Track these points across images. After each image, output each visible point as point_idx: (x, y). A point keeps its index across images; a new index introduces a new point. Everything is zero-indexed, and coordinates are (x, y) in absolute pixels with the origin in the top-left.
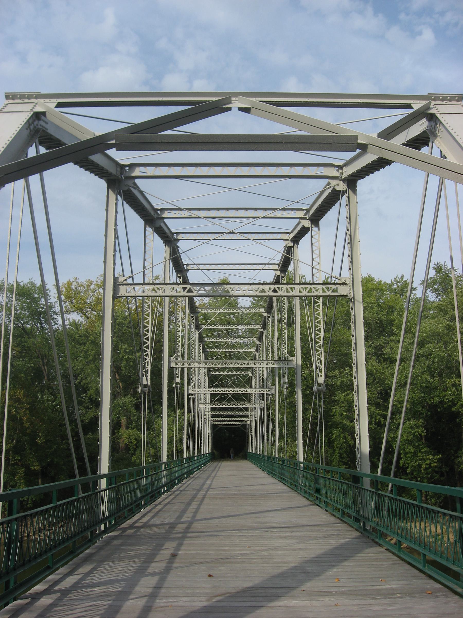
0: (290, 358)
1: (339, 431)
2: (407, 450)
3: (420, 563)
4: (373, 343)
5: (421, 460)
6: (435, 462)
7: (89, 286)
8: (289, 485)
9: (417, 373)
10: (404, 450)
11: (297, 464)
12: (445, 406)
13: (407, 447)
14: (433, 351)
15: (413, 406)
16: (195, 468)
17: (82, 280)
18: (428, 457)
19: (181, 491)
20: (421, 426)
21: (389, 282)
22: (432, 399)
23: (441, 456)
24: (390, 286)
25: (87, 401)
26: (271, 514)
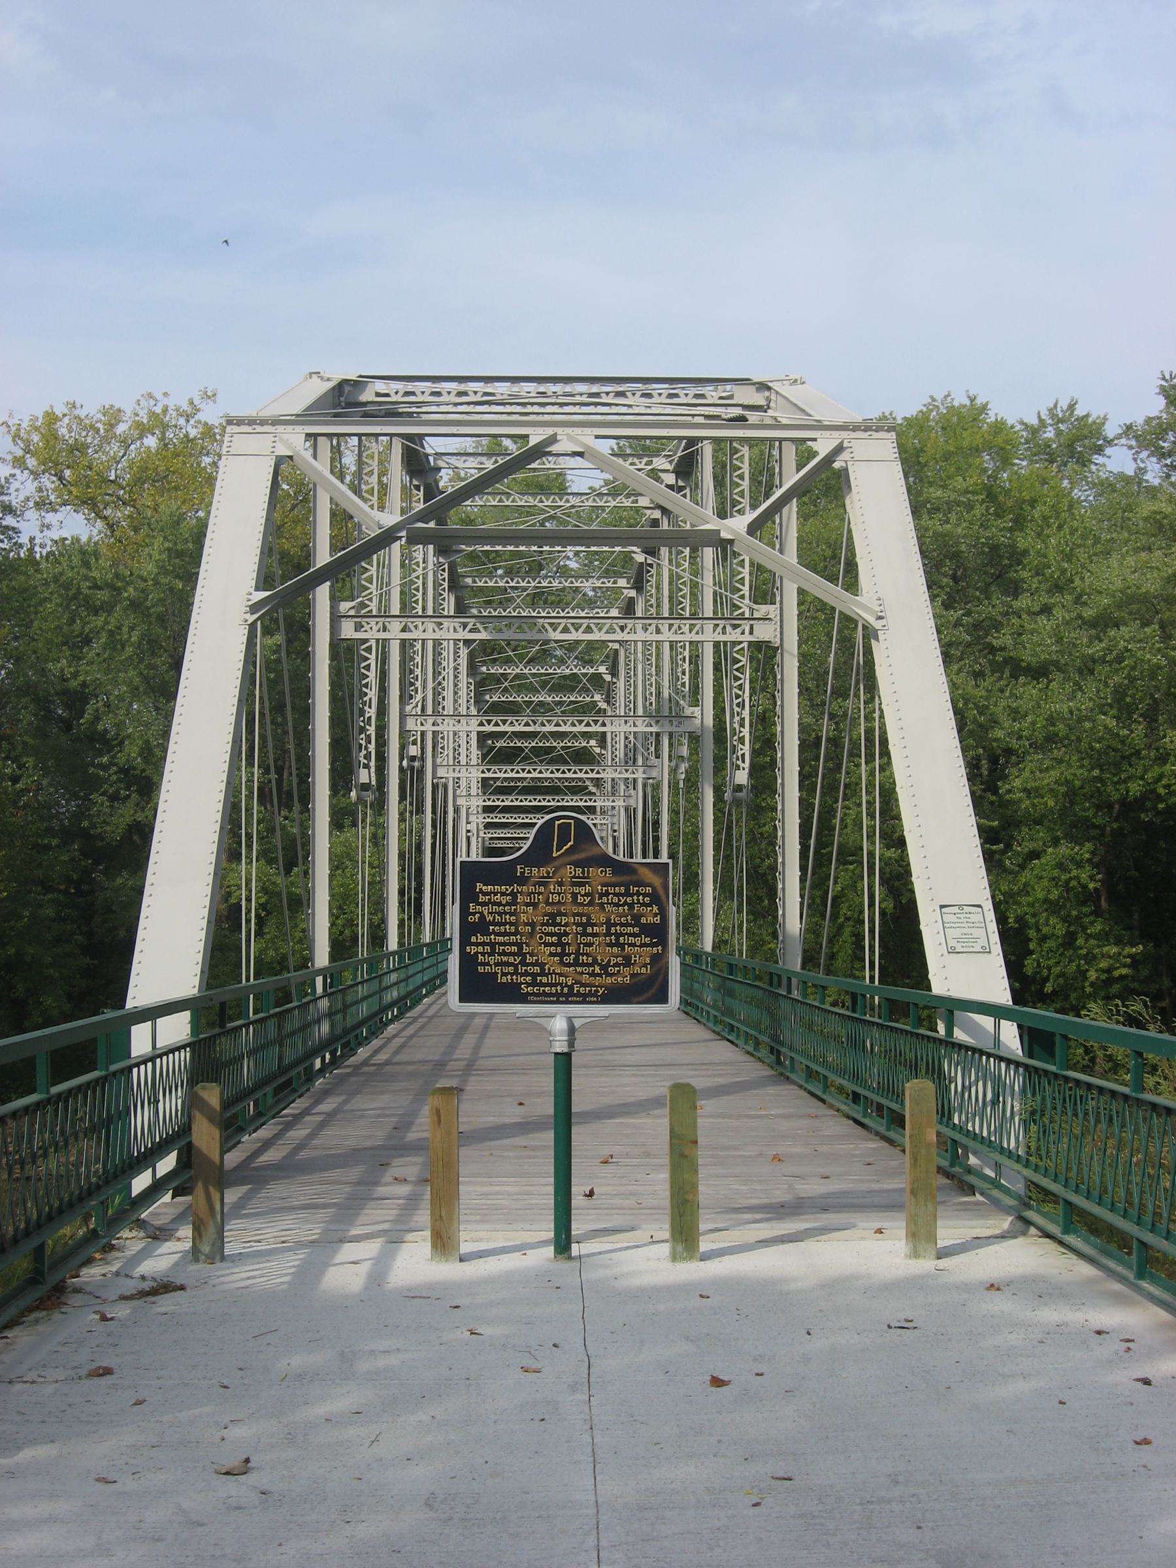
0: (688, 711)
1: (853, 871)
2: (1045, 930)
3: (1131, 1268)
4: (968, 613)
5: (1085, 957)
6: (1124, 966)
7: (111, 426)
8: (710, 1025)
9: (1079, 710)
10: (1038, 930)
11: (779, 977)
12: (1161, 806)
13: (1047, 920)
14: (1127, 650)
15: (1072, 803)
16: (424, 985)
17: (91, 409)
18: (1106, 949)
19: (431, 1018)
20: (1088, 860)
21: (1034, 421)
22: (1123, 786)
23: (1141, 947)
24: (1034, 431)
25: (114, 777)
26: (628, 1050)
